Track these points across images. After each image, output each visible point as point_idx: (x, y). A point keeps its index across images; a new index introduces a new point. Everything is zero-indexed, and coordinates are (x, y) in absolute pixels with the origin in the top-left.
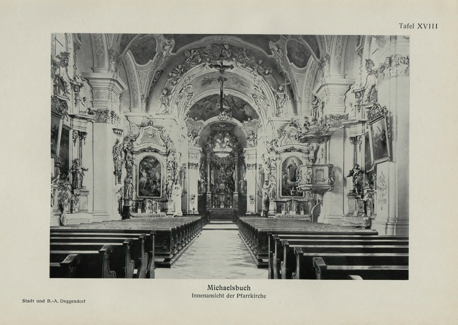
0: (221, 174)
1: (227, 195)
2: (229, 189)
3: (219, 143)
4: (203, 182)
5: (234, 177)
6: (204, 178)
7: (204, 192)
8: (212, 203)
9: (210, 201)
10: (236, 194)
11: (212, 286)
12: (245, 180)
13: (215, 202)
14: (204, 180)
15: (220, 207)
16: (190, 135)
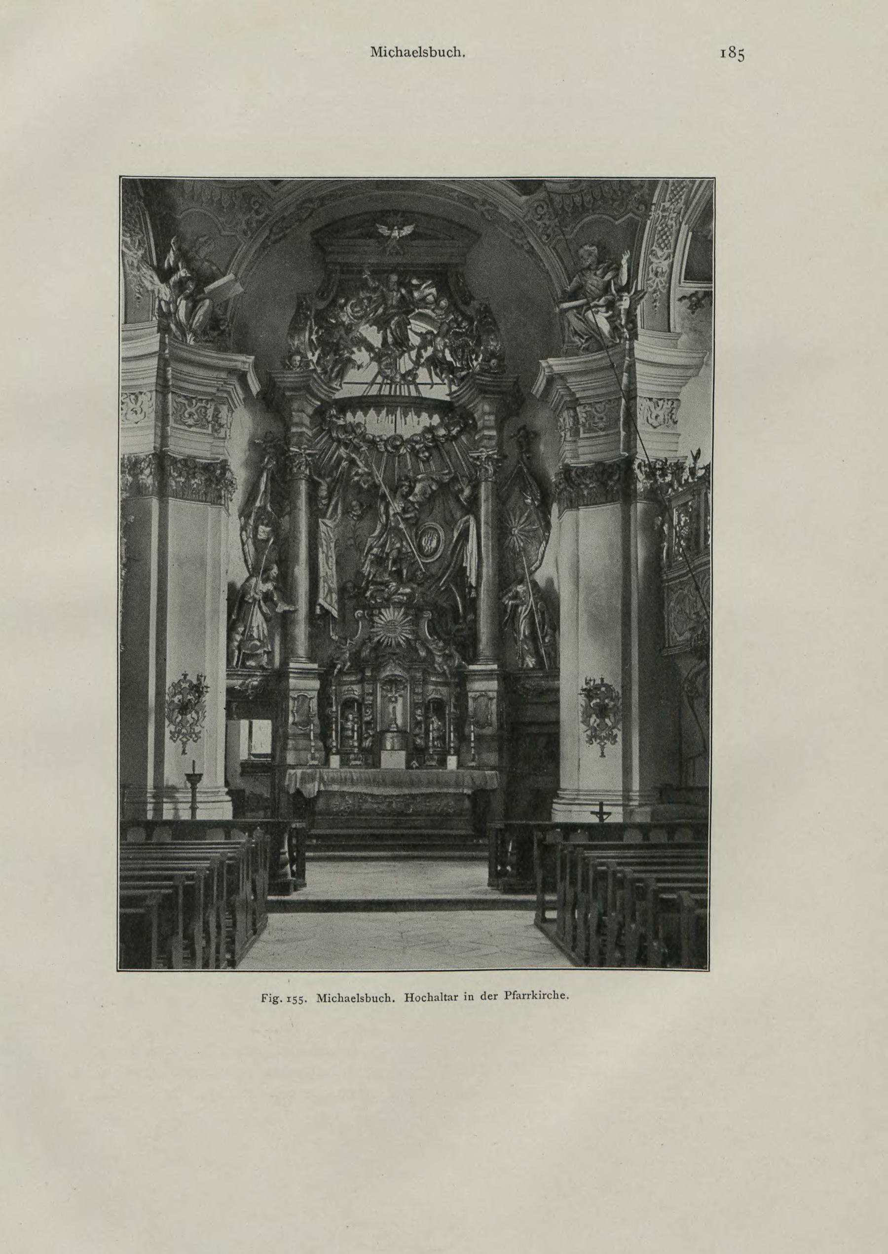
0: (383, 546)
1: (425, 682)
2: (436, 646)
3: (370, 348)
4: (267, 597)
5: (471, 564)
6: (267, 570)
7: (271, 661)
8: (324, 736)
9: (308, 723)
10: (487, 675)
11: (325, 995)
12: (542, 583)
13: (343, 729)
14: (269, 586)
15: (376, 764)
16: (173, 270)
